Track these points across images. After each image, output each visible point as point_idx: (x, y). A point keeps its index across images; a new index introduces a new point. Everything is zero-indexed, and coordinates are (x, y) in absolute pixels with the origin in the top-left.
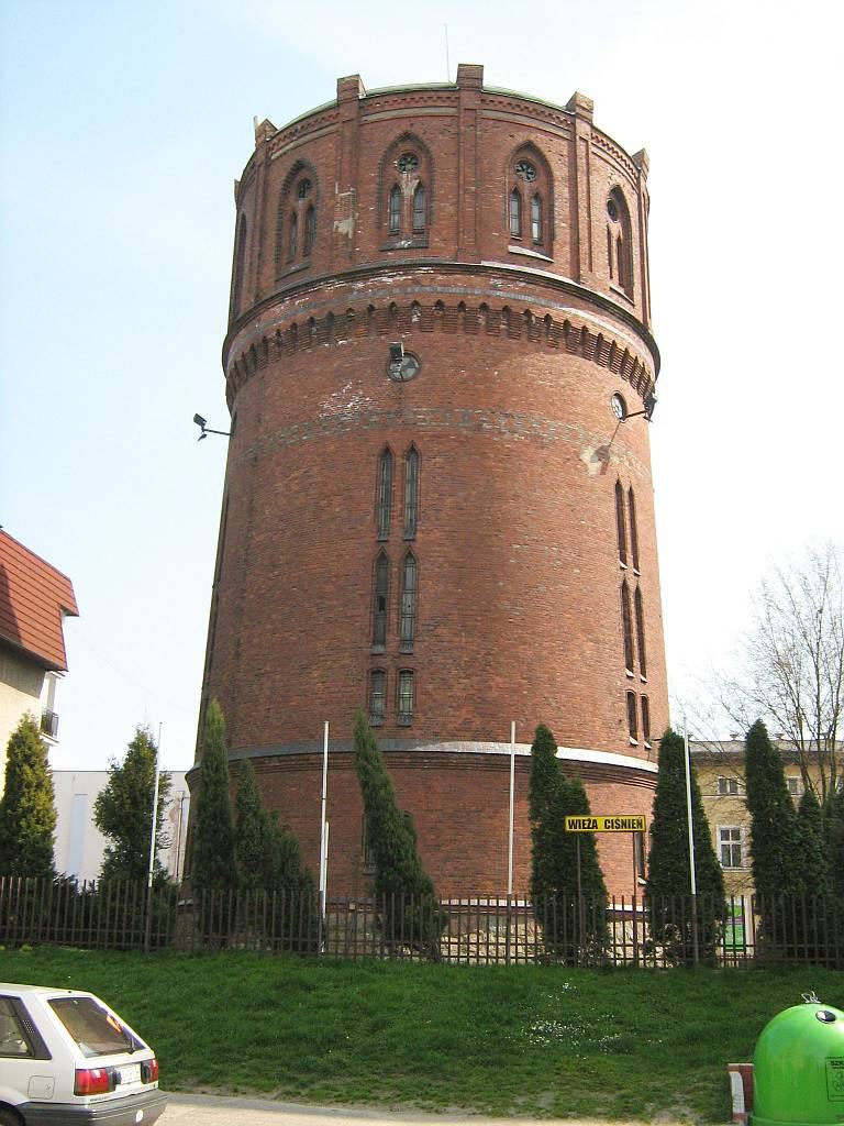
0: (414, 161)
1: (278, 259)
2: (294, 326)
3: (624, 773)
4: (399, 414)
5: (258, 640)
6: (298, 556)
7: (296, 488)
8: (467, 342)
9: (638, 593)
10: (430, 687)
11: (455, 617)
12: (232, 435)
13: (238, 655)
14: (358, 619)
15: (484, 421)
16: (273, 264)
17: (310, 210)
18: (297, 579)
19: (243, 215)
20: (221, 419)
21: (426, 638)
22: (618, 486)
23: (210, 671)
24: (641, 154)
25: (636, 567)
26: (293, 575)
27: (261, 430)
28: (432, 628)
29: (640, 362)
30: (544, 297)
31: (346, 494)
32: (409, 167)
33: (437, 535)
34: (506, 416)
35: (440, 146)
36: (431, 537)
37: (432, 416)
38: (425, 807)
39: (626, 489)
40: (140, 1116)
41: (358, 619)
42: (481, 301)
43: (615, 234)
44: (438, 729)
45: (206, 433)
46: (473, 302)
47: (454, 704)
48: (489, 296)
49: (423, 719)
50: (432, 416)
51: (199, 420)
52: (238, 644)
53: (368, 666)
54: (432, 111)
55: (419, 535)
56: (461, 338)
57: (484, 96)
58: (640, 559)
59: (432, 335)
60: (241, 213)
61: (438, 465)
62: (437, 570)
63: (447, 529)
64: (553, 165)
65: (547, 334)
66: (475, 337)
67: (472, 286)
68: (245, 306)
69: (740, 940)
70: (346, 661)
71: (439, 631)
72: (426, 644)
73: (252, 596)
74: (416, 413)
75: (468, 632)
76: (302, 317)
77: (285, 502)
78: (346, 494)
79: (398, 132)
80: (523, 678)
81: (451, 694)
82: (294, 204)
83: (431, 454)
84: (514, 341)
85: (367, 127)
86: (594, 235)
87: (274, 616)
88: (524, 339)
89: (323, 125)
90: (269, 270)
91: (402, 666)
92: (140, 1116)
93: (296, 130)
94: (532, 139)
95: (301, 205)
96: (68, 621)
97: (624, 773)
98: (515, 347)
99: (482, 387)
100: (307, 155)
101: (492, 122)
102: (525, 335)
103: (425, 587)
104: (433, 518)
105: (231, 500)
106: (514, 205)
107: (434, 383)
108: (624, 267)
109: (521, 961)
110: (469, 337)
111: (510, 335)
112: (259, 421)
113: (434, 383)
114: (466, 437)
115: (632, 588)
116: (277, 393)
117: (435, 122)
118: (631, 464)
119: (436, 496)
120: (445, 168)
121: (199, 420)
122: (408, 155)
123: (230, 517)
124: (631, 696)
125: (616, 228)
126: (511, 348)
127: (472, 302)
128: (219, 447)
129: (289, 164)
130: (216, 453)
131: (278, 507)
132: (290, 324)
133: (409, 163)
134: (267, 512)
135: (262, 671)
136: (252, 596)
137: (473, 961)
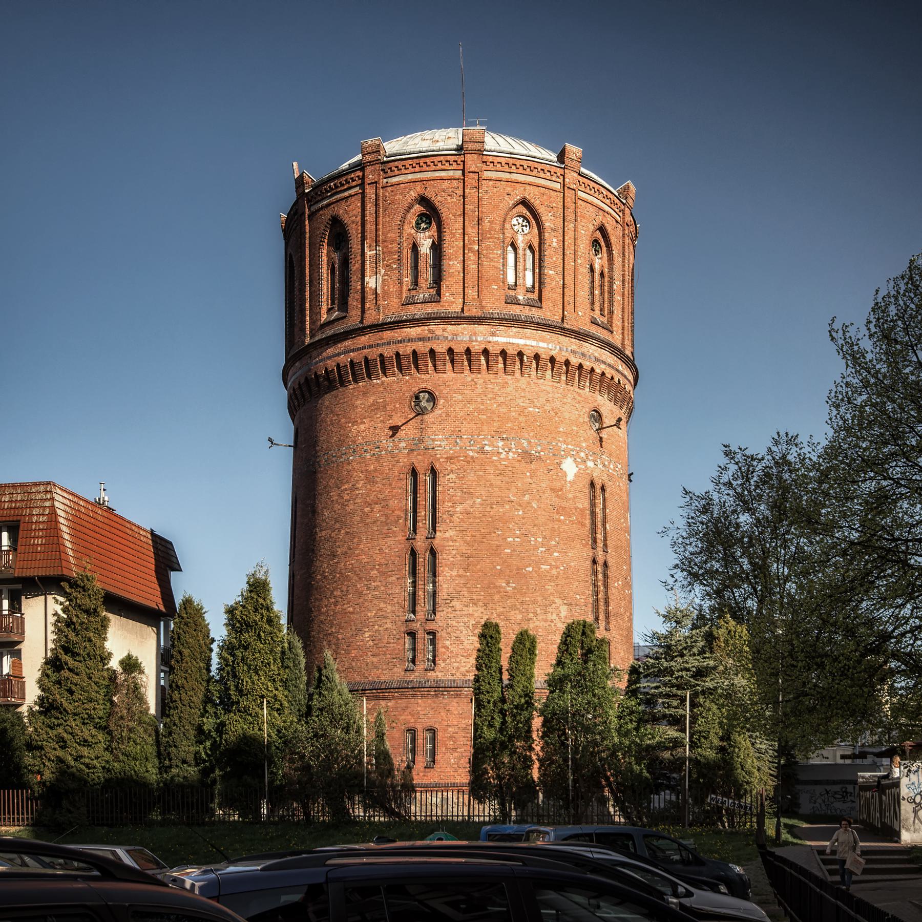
4: (421, 441)
8: (473, 380)
10: (448, 643)
11: (466, 593)
22: (592, 485)
31: (383, 503)
33: (450, 533)
34: (503, 439)
35: (449, 207)
36: (447, 535)
38: (446, 723)
42: (483, 346)
43: (597, 267)
48: (489, 342)
49: (443, 665)
51: (270, 440)
53: (403, 629)
54: (443, 174)
56: (467, 376)
59: (445, 376)
62: (452, 559)
66: (479, 376)
67: (475, 334)
69: (429, 814)
70: (389, 625)
71: (453, 603)
74: (433, 440)
75: (475, 604)
78: (383, 503)
79: (413, 194)
83: (446, 472)
84: (510, 377)
85: (389, 189)
96: (173, 575)
101: (491, 183)
106: (511, 257)
107: (448, 415)
109: (434, 818)
110: (473, 376)
113: (448, 415)
114: (472, 457)
118: (604, 466)
119: (450, 504)
120: (453, 226)
123: (295, 602)
125: (599, 263)
127: (476, 348)
137: (428, 818)
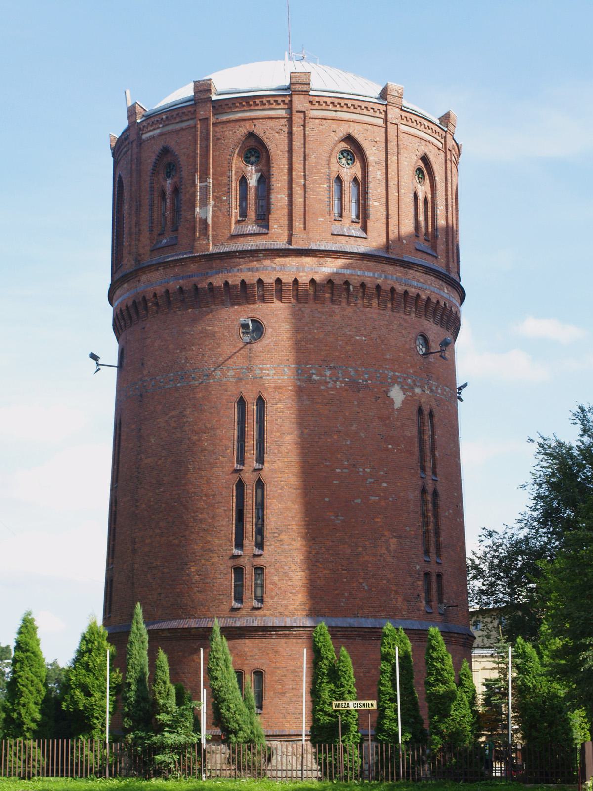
0: (257, 155)
1: (151, 230)
2: (167, 292)
3: (420, 634)
5: (150, 540)
6: (177, 478)
7: (173, 424)
9: (435, 494)
10: (276, 579)
12: (120, 366)
13: (134, 551)
14: (223, 529)
15: (313, 374)
16: (148, 235)
17: (176, 191)
18: (177, 496)
19: (120, 177)
20: (110, 350)
21: (273, 543)
23: (113, 558)
24: (446, 119)
25: (435, 473)
26: (174, 493)
27: (145, 372)
28: (276, 535)
29: (442, 303)
30: (360, 269)
32: (253, 159)
37: (274, 372)
39: (426, 413)
40: (482, 745)
41: (223, 529)
43: (421, 197)
44: (282, 610)
45: (100, 367)
46: (304, 278)
47: (294, 591)
50: (274, 372)
51: (94, 357)
52: (134, 543)
55: (266, 465)
57: (311, 99)
58: (438, 466)
60: (117, 174)
61: (279, 410)
63: (286, 460)
64: (368, 152)
65: (363, 297)
66: (306, 305)
68: (129, 264)
72: (272, 547)
73: (144, 506)
74: (262, 369)
76: (174, 285)
77: (166, 434)
80: (343, 570)
81: (290, 584)
82: (163, 184)
84: (336, 306)
86: (402, 206)
87: (162, 524)
88: (344, 304)
89: (183, 119)
90: (145, 239)
91: (255, 563)
92: (482, 745)
93: (162, 119)
94: (350, 132)
95: (168, 184)
97: (420, 634)
98: (337, 311)
99: (312, 346)
100: (172, 144)
101: (317, 121)
102: (345, 300)
103: (271, 504)
104: (276, 451)
105: (122, 423)
108: (265, 629)
110: (301, 305)
111: (332, 301)
112: (143, 365)
115: (430, 489)
116: (156, 344)
117: (271, 123)
118: (432, 391)
119: (278, 434)
121: (94, 357)
122: (253, 149)
124: (427, 575)
126: (334, 312)
128: (110, 377)
129: (157, 148)
130: (108, 381)
131: (161, 438)
132: (163, 290)
133: (253, 156)
134: (153, 441)
135: (154, 565)
136: (144, 506)
